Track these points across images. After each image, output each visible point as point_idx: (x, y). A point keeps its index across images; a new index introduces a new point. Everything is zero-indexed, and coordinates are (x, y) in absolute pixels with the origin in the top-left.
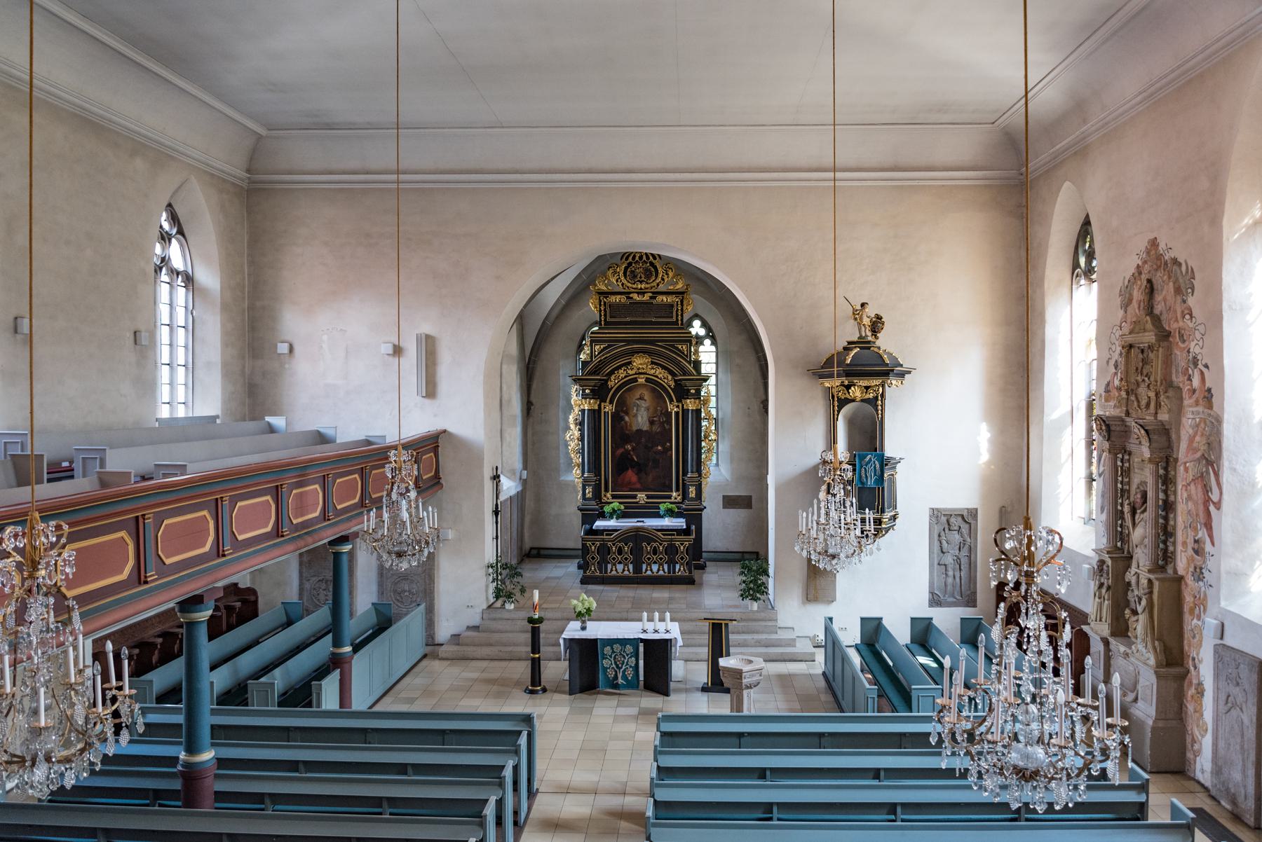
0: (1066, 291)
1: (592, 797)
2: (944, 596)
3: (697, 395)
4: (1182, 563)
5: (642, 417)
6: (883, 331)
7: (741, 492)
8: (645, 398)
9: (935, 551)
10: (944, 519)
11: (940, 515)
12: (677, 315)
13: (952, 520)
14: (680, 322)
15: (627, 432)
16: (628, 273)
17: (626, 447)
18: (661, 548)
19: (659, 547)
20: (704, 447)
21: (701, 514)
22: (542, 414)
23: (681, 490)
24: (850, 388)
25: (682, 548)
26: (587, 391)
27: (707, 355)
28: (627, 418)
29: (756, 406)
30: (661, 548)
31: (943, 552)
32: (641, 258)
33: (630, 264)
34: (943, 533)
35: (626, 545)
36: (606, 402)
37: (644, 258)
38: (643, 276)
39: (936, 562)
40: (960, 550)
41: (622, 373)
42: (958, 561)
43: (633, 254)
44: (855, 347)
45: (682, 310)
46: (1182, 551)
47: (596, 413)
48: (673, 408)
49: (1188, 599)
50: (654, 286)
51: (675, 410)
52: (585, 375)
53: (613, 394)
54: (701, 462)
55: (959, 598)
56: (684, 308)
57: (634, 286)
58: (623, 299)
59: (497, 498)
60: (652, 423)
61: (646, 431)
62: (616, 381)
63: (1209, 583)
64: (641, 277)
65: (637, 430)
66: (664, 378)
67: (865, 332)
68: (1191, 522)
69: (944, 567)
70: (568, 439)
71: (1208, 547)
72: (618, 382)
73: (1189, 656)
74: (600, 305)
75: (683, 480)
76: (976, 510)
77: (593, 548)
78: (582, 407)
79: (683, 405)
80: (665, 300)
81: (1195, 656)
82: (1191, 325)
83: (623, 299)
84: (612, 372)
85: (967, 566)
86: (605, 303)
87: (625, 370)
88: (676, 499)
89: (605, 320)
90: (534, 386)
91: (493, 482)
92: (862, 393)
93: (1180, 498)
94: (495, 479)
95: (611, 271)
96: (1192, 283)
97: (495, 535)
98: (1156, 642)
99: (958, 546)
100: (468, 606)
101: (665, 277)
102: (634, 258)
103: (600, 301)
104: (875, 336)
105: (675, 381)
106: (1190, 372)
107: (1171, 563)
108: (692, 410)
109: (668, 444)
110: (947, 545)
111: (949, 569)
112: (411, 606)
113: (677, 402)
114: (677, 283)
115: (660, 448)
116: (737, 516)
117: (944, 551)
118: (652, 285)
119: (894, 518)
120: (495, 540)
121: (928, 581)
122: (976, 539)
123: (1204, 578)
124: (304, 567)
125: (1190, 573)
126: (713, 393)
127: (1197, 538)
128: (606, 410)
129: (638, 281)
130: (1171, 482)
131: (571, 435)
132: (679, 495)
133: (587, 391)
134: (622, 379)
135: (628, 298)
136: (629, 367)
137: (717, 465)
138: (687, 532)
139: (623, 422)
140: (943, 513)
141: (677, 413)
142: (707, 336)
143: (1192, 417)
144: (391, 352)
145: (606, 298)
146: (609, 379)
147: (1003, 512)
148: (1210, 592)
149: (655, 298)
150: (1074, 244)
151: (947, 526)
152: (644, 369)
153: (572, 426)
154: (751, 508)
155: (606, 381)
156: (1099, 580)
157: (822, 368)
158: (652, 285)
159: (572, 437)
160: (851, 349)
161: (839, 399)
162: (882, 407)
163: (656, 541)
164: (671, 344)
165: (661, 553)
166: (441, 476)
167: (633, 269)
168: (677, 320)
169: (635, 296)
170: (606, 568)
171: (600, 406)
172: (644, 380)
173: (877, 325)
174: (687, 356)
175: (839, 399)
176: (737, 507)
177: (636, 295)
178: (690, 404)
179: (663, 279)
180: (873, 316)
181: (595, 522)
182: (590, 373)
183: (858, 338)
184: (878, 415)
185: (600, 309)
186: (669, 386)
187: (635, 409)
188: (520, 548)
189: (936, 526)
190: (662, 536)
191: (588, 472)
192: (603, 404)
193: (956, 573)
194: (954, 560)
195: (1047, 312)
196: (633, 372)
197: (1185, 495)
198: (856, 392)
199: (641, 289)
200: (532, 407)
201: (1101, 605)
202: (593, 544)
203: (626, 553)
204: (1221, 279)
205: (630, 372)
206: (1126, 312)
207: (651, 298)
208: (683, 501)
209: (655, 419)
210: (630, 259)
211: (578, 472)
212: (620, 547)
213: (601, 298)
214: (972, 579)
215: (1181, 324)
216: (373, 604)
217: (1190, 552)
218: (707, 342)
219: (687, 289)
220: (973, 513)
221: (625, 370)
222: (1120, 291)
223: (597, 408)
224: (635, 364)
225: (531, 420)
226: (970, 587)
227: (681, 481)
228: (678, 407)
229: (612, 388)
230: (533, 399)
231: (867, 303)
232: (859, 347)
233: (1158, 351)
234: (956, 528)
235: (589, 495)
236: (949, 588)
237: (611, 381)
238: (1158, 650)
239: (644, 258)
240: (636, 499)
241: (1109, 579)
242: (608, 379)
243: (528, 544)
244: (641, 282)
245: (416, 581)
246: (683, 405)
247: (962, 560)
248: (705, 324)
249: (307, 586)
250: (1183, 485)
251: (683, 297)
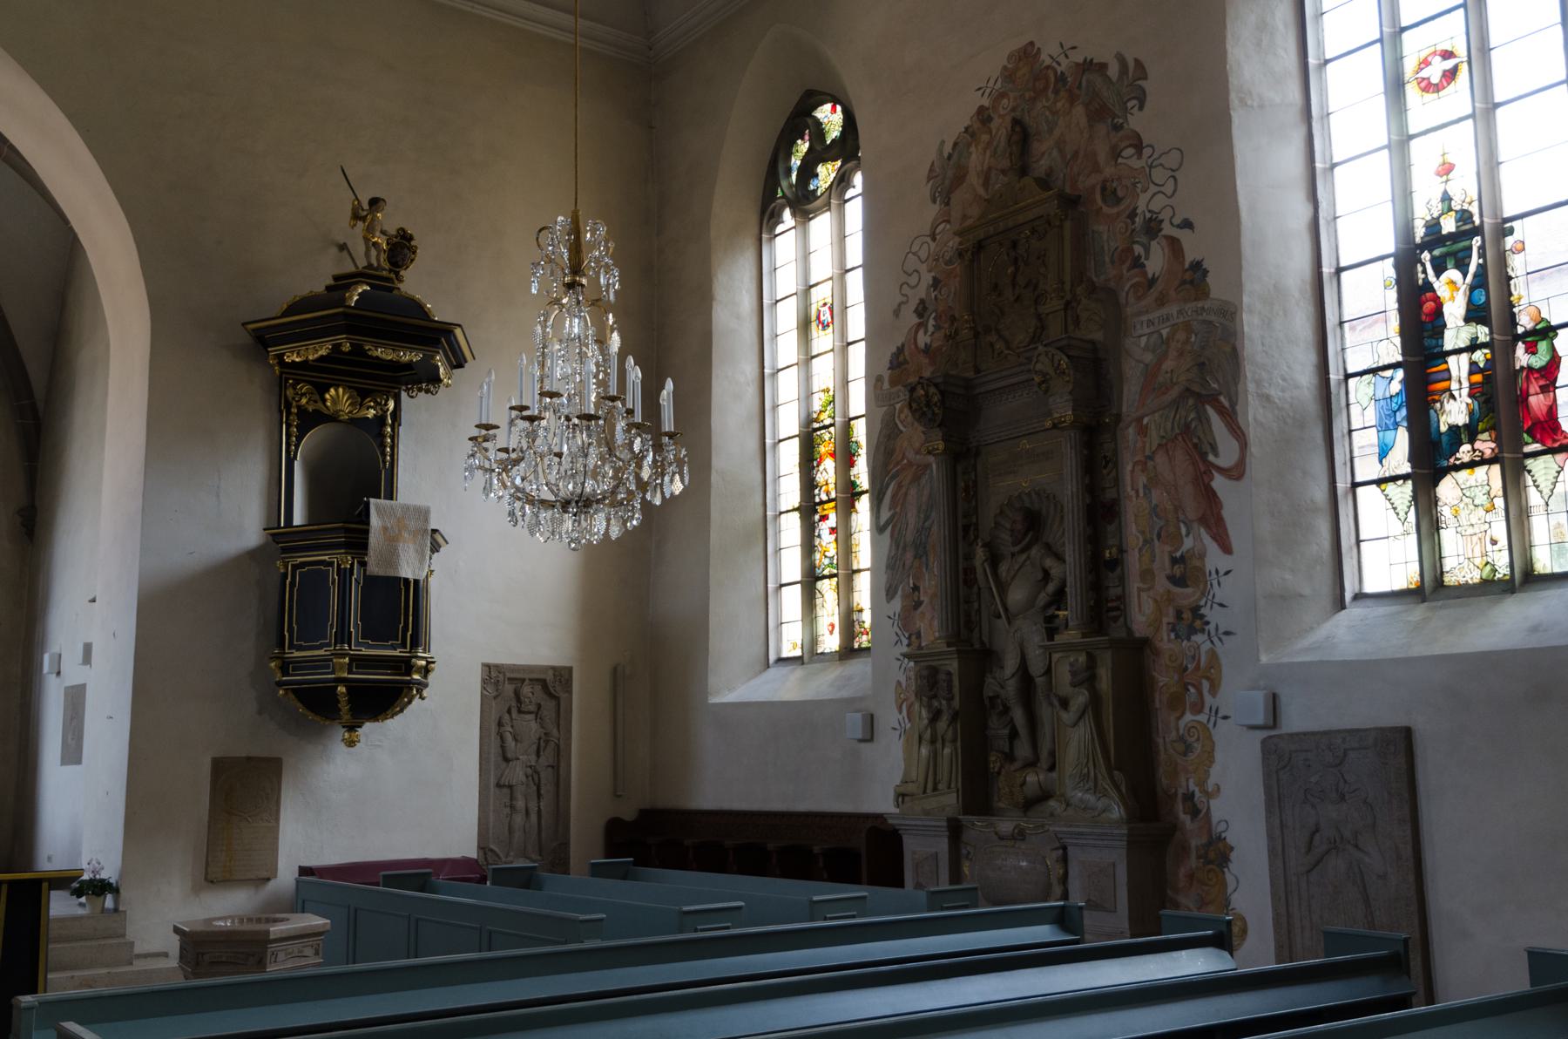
0: (750, 244)
4: (1142, 613)
10: (509, 689)
13: (526, 690)
24: (328, 391)
31: (506, 760)
34: (507, 717)
39: (493, 781)
40: (538, 755)
42: (534, 775)
46: (1139, 590)
49: (1164, 679)
63: (1221, 630)
67: (378, 259)
68: (1161, 528)
71: (1214, 559)
73: (1176, 794)
81: (1192, 787)
82: (1136, 164)
93: (1129, 489)
96: (1140, 86)
98: (1116, 772)
99: (535, 747)
104: (397, 274)
106: (1138, 249)
107: (1116, 619)
110: (513, 743)
111: (519, 796)
117: (509, 755)
122: (569, 731)
123: (1208, 623)
125: (1165, 627)
127: (1178, 554)
130: (1107, 463)
140: (508, 675)
143: (1147, 331)
147: (618, 678)
148: (1225, 650)
150: (768, 157)
151: (514, 704)
156: (929, 706)
157: (284, 315)
161: (302, 411)
162: (393, 441)
173: (401, 248)
184: (384, 454)
193: (530, 805)
194: (527, 777)
195: (715, 281)
197: (1142, 480)
201: (934, 756)
204: (1225, 52)
206: (947, 204)
214: (561, 815)
215: (1109, 171)
217: (1162, 584)
222: (931, 170)
231: (383, 200)
233: (1061, 227)
234: (532, 708)
236: (518, 835)
238: (1124, 790)
241: (952, 698)
250: (1135, 464)
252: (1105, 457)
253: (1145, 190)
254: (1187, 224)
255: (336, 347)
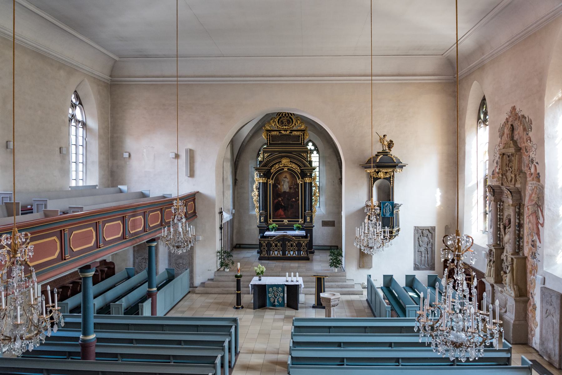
0: (475, 129)
1: (264, 355)
2: (421, 265)
3: (311, 176)
4: (526, 251)
5: (286, 186)
6: (393, 148)
7: (330, 219)
8: (287, 177)
9: (417, 246)
10: (420, 231)
11: (418, 229)
12: (302, 140)
13: (424, 232)
14: (303, 144)
15: (279, 192)
16: (280, 122)
17: (279, 199)
18: (294, 244)
19: (293, 244)
20: (314, 199)
21: (312, 229)
22: (241, 184)
23: (303, 218)
24: (379, 173)
25: (304, 244)
26: (261, 174)
27: (315, 158)
28: (279, 186)
29: (337, 181)
30: (294, 244)
31: (420, 246)
32: (285, 115)
33: (281, 118)
34: (420, 237)
35: (279, 243)
36: (270, 179)
37: (287, 115)
38: (286, 123)
39: (417, 251)
40: (427, 245)
41: (277, 166)
42: (427, 250)
43: (282, 113)
44: (381, 155)
45: (304, 138)
46: (526, 245)
47: (266, 184)
48: (299, 182)
49: (529, 267)
50: (291, 128)
51: (301, 182)
52: (261, 167)
53: (273, 175)
54: (312, 206)
55: (427, 266)
56: (305, 137)
57: (283, 127)
58: (277, 133)
59: (221, 222)
60: (290, 188)
61: (288, 192)
62: (274, 170)
63: (538, 260)
64: (285, 123)
65: (284, 192)
66: (296, 168)
67: (385, 148)
68: (530, 233)
69: (420, 252)
70: (253, 195)
72: (275, 170)
73: (530, 292)
74: (267, 136)
75: (304, 214)
76: (435, 227)
77: (264, 244)
78: (259, 181)
79: (304, 181)
80: (296, 133)
81: (532, 292)
82: (530, 145)
83: (277, 133)
84: (273, 166)
85: (431, 252)
86: (269, 135)
87: (278, 165)
88: (301, 222)
89: (269, 143)
90: (238, 172)
91: (220, 215)
92: (384, 175)
93: (525, 222)
94: (220, 213)
95: (272, 121)
96: (531, 126)
97: (220, 238)
98: (515, 286)
99: (427, 243)
100: (208, 270)
101: (296, 123)
102: (282, 115)
103: (267, 134)
105: (301, 170)
106: (530, 166)
107: (521, 251)
108: (308, 183)
109: (298, 198)
110: (422, 243)
111: (423, 253)
112: (183, 270)
113: (302, 179)
114: (301, 126)
115: (294, 199)
116: (328, 230)
117: (420, 245)
118: (290, 127)
119: (398, 231)
120: (220, 241)
121: (413, 259)
122: (435, 240)
123: (536, 257)
124: (135, 252)
125: (530, 255)
126: (318, 175)
127: (533, 240)
128: (270, 183)
129: (284, 125)
130: (522, 215)
131: (254, 194)
132: (302, 221)
133: (261, 174)
134: (277, 169)
135: (280, 133)
136: (280, 164)
137: (319, 207)
138: (306, 237)
139: (277, 188)
140: (420, 228)
141: (302, 184)
142: (315, 150)
143: (531, 186)
144: (174, 157)
145: (270, 133)
146: (271, 169)
147: (447, 228)
148: (539, 264)
149: (292, 133)
150: (478, 109)
151: (422, 234)
152: (287, 164)
153: (255, 190)
154: (335, 226)
155: (270, 170)
157: (366, 164)
158: (290, 127)
159: (255, 195)
160: (379, 156)
161: (374, 178)
162: (393, 181)
163: (292, 241)
164: (299, 153)
165: (294, 246)
166: (196, 212)
167: (282, 120)
168: (302, 142)
169: (283, 132)
170: (270, 253)
171: (267, 181)
172: (287, 169)
173: (390, 145)
174: (306, 159)
175: (374, 178)
176: (328, 226)
177: (283, 131)
178: (307, 180)
179: (295, 124)
180: (389, 141)
181: (265, 232)
182: (263, 166)
183: (382, 151)
184: (391, 185)
185: (267, 138)
186: (298, 172)
187: (283, 182)
188: (232, 244)
189: (417, 234)
190: (295, 239)
191: (262, 210)
192: (268, 180)
193: (426, 255)
194: (425, 249)
195: (466, 139)
196: (282, 166)
197: (528, 220)
198: (381, 175)
199: (285, 129)
200: (237, 181)
202: (264, 242)
203: (279, 246)
204: (544, 124)
205: (281, 166)
206: (501, 139)
207: (290, 133)
208: (304, 223)
209: (292, 186)
210: (281, 115)
211: (257, 210)
212: (276, 243)
213: (268, 133)
214: (433, 258)
215: (526, 144)
216: (166, 269)
217: (530, 246)
218: (315, 152)
219: (306, 129)
220: (433, 228)
221: (278, 165)
222: (499, 130)
223: (266, 182)
224: (283, 162)
225: (236, 187)
226: (432, 261)
227: (303, 214)
228: (302, 181)
229: (273, 173)
230: (237, 178)
231: (386, 135)
232: (382, 155)
233: (516, 156)
234: (426, 235)
235: (262, 221)
236: (423, 262)
237: (272, 170)
238: (516, 290)
239: (287, 115)
240: (283, 222)
241: (494, 258)
242: (271, 169)
243: (235, 242)
244: (285, 126)
245: (185, 259)
246: (304, 181)
247: (428, 249)
248: (314, 144)
249: (137, 261)
250: (527, 216)
251: (304, 132)
252: (521, 213)
253: (531, 152)
254: (537, 163)
255: (375, 170)
